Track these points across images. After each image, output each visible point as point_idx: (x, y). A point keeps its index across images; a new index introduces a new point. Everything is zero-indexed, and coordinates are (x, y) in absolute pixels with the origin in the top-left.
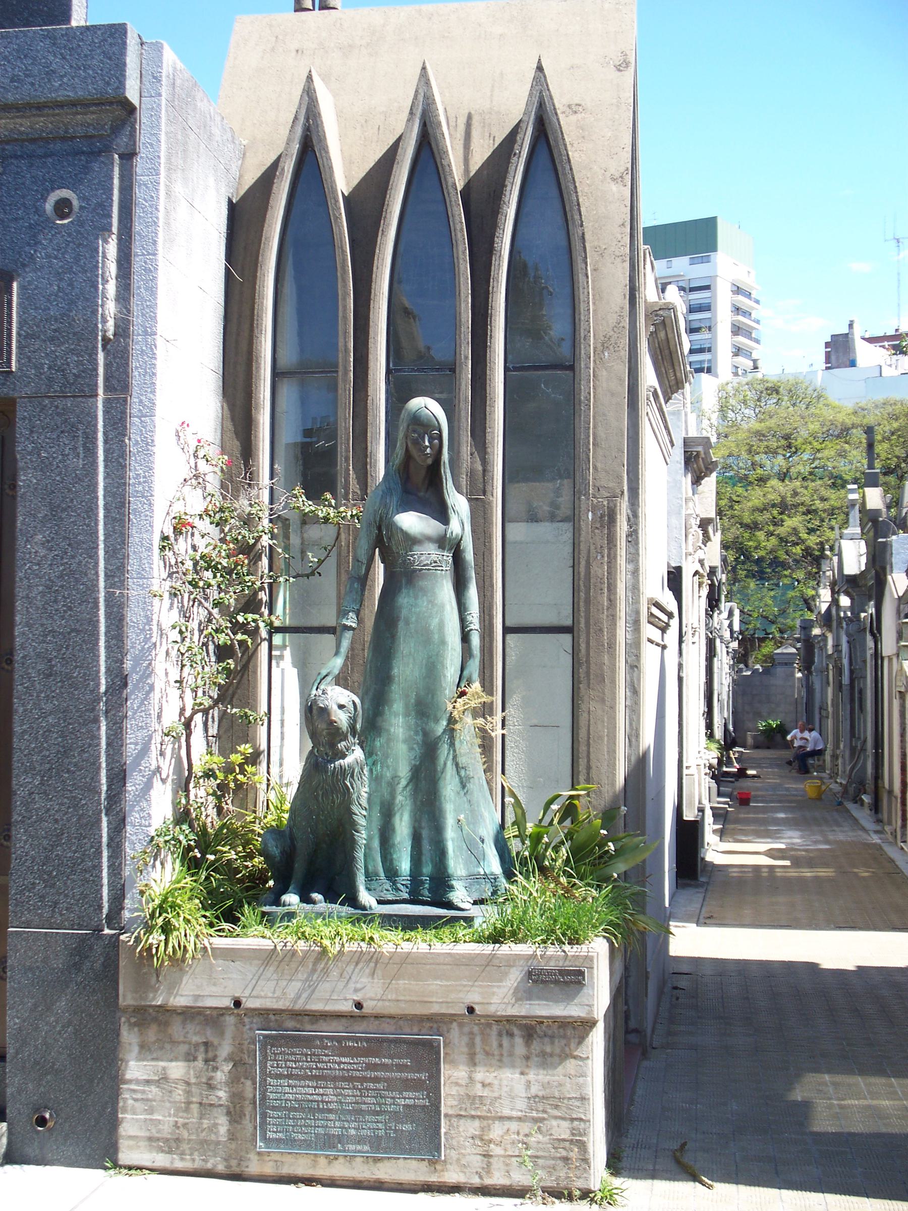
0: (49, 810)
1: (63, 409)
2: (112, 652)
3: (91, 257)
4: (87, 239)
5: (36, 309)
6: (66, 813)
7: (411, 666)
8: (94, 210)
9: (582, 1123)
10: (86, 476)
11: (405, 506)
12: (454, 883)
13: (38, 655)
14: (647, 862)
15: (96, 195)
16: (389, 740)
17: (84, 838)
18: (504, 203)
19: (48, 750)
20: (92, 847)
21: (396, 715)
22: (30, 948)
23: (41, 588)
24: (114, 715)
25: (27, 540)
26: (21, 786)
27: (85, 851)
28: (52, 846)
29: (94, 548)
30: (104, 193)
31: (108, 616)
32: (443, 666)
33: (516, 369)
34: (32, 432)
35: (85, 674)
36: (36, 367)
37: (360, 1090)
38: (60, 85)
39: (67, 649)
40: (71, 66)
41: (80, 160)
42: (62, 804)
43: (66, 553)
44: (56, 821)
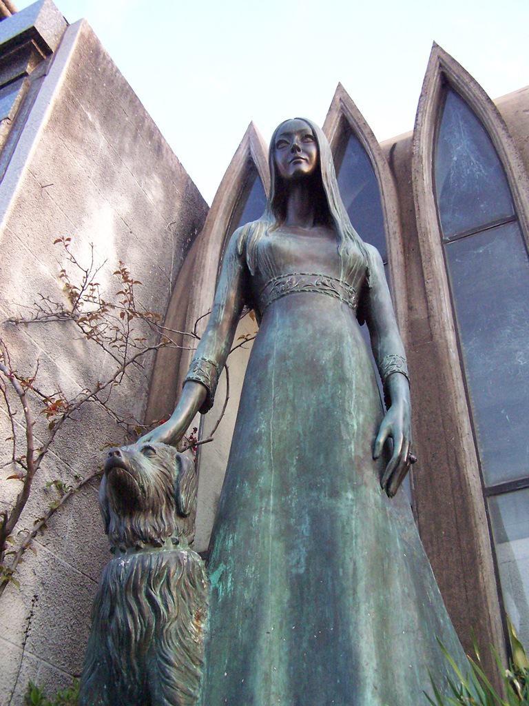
11: (252, 276)
14: (397, 146)
16: (249, 534)
21: (264, 494)
32: (344, 411)
33: (453, 239)
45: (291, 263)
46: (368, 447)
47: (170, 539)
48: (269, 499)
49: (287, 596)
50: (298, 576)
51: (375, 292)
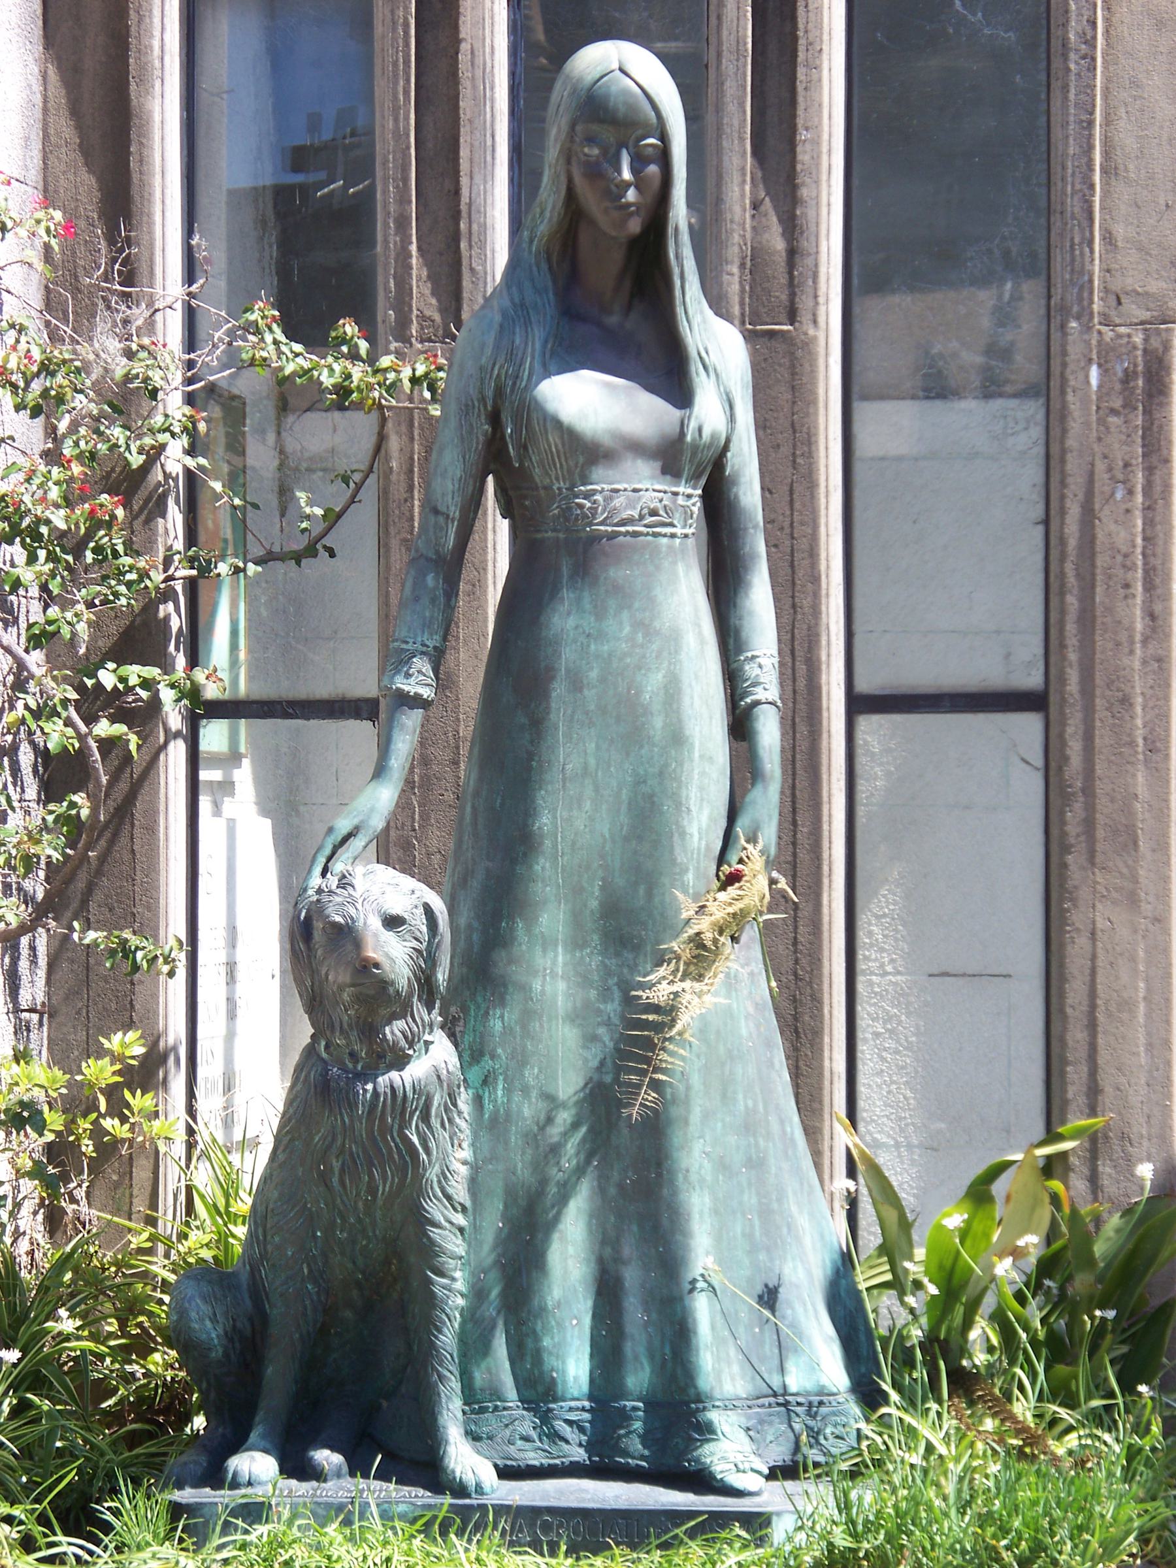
7: (588, 805)
12: (713, 1416)
16: (528, 1015)
21: (547, 944)
48: (556, 956)
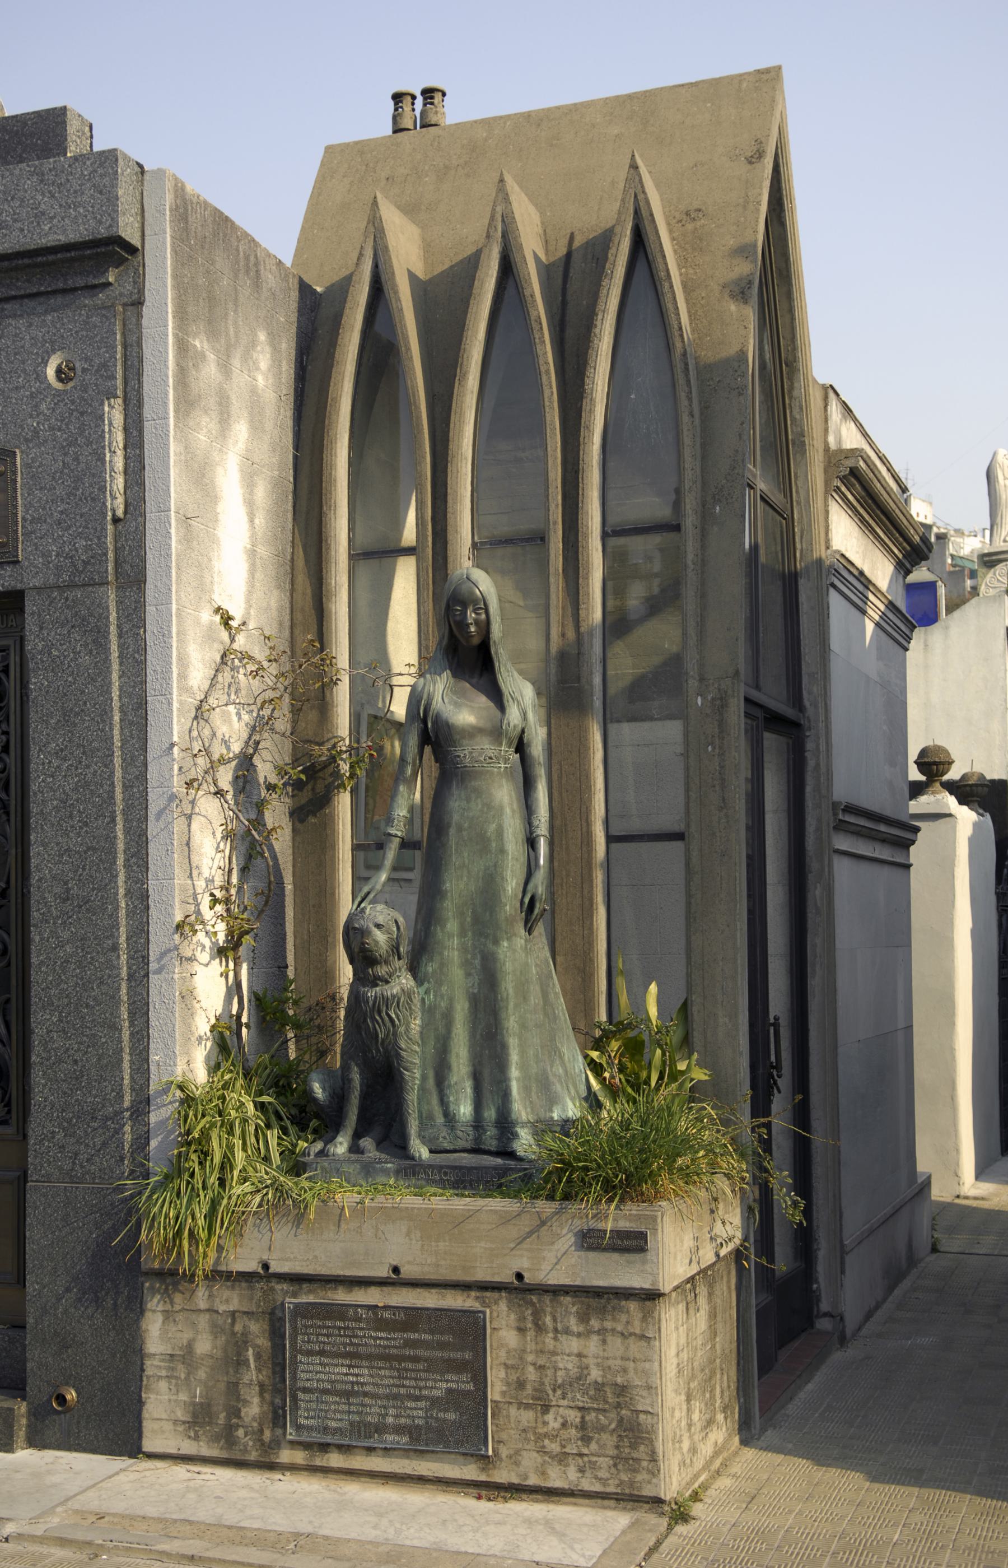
0: (68, 1049)
1: (73, 601)
2: (133, 871)
3: (96, 426)
4: (91, 405)
5: (41, 489)
6: (86, 1053)
7: (465, 879)
8: (97, 371)
9: (649, 1416)
10: (99, 674)
12: (518, 1130)
13: (54, 878)
15: (99, 354)
16: (442, 965)
17: (105, 1081)
18: (595, 336)
19: (66, 983)
20: (113, 1090)
21: (450, 936)
22: (50, 1205)
23: (55, 803)
24: (135, 942)
25: (40, 750)
26: (39, 1023)
27: (106, 1094)
28: (71, 1090)
29: (109, 756)
30: (107, 352)
31: (127, 831)
32: (503, 878)
34: (41, 628)
35: (102, 897)
36: (43, 555)
37: (398, 1370)
38: (50, 228)
39: (84, 869)
40: (61, 206)
41: (80, 315)
42: (81, 1043)
43: (80, 762)
44: (76, 1062)
45: (464, 738)
46: (518, 905)
47: (280, 784)
49: (467, 1005)
50: (473, 994)
51: (529, 745)
